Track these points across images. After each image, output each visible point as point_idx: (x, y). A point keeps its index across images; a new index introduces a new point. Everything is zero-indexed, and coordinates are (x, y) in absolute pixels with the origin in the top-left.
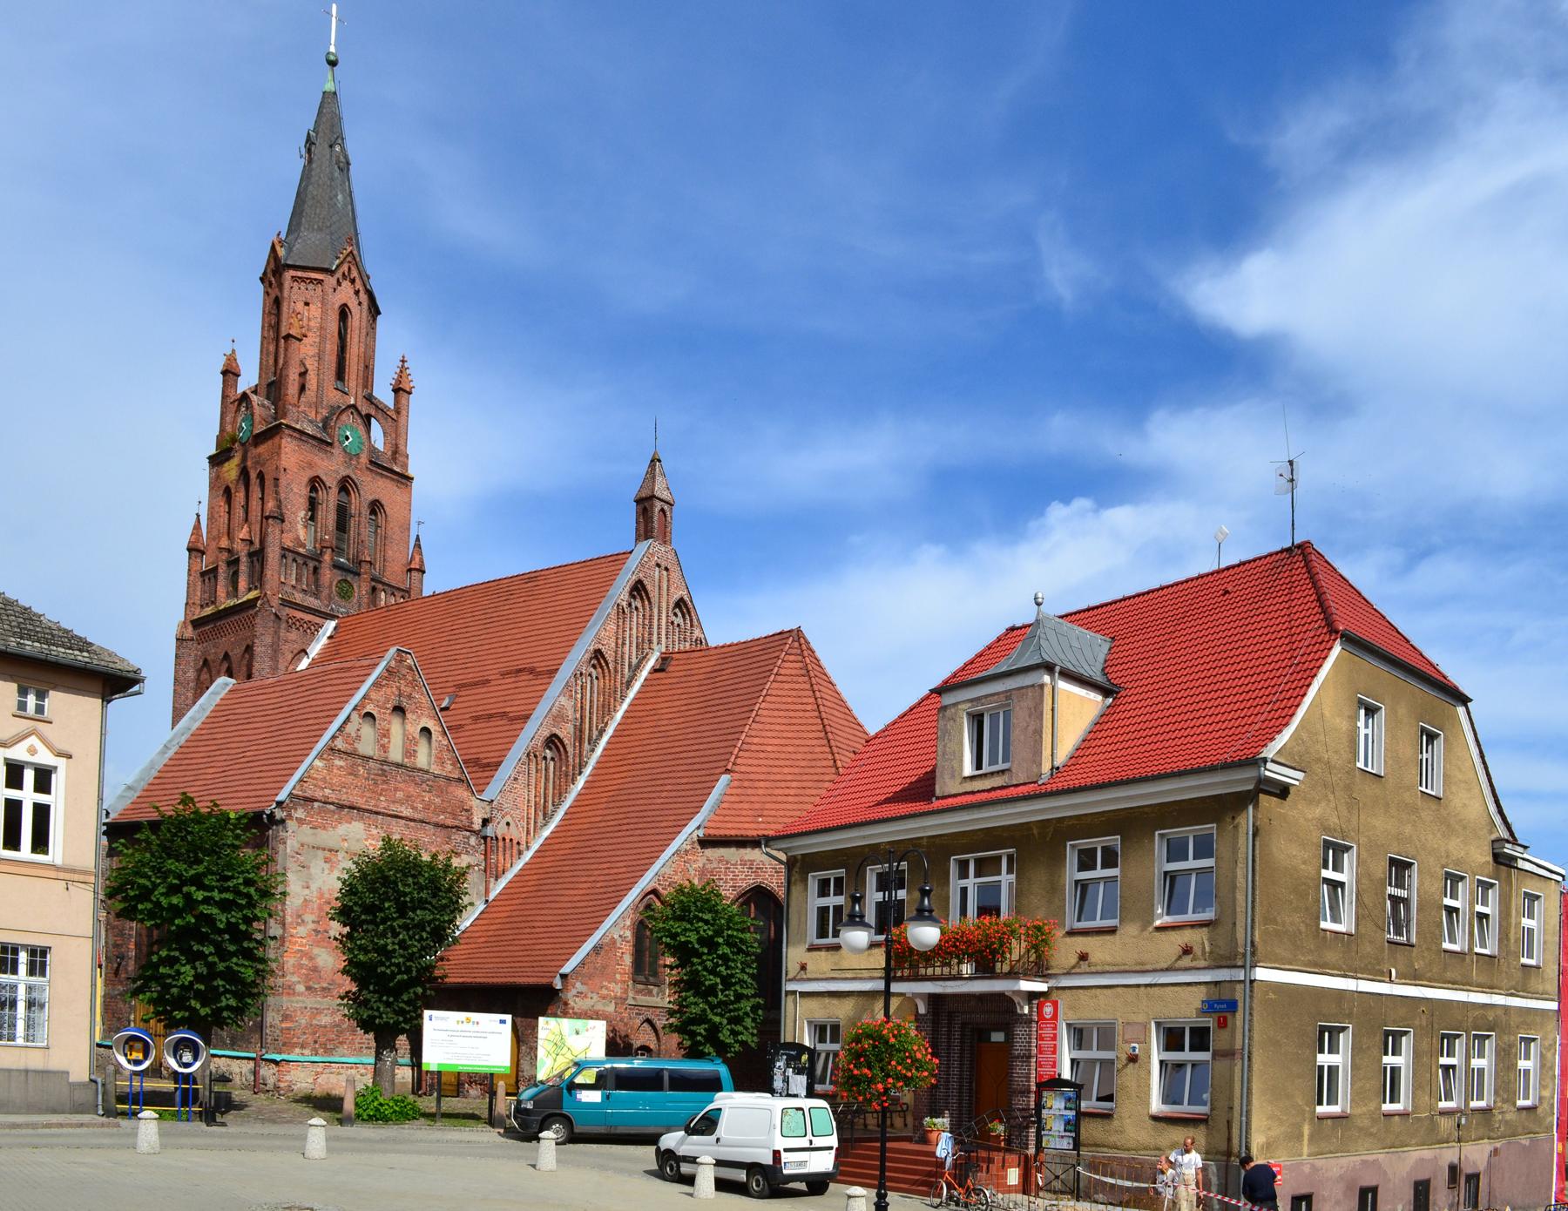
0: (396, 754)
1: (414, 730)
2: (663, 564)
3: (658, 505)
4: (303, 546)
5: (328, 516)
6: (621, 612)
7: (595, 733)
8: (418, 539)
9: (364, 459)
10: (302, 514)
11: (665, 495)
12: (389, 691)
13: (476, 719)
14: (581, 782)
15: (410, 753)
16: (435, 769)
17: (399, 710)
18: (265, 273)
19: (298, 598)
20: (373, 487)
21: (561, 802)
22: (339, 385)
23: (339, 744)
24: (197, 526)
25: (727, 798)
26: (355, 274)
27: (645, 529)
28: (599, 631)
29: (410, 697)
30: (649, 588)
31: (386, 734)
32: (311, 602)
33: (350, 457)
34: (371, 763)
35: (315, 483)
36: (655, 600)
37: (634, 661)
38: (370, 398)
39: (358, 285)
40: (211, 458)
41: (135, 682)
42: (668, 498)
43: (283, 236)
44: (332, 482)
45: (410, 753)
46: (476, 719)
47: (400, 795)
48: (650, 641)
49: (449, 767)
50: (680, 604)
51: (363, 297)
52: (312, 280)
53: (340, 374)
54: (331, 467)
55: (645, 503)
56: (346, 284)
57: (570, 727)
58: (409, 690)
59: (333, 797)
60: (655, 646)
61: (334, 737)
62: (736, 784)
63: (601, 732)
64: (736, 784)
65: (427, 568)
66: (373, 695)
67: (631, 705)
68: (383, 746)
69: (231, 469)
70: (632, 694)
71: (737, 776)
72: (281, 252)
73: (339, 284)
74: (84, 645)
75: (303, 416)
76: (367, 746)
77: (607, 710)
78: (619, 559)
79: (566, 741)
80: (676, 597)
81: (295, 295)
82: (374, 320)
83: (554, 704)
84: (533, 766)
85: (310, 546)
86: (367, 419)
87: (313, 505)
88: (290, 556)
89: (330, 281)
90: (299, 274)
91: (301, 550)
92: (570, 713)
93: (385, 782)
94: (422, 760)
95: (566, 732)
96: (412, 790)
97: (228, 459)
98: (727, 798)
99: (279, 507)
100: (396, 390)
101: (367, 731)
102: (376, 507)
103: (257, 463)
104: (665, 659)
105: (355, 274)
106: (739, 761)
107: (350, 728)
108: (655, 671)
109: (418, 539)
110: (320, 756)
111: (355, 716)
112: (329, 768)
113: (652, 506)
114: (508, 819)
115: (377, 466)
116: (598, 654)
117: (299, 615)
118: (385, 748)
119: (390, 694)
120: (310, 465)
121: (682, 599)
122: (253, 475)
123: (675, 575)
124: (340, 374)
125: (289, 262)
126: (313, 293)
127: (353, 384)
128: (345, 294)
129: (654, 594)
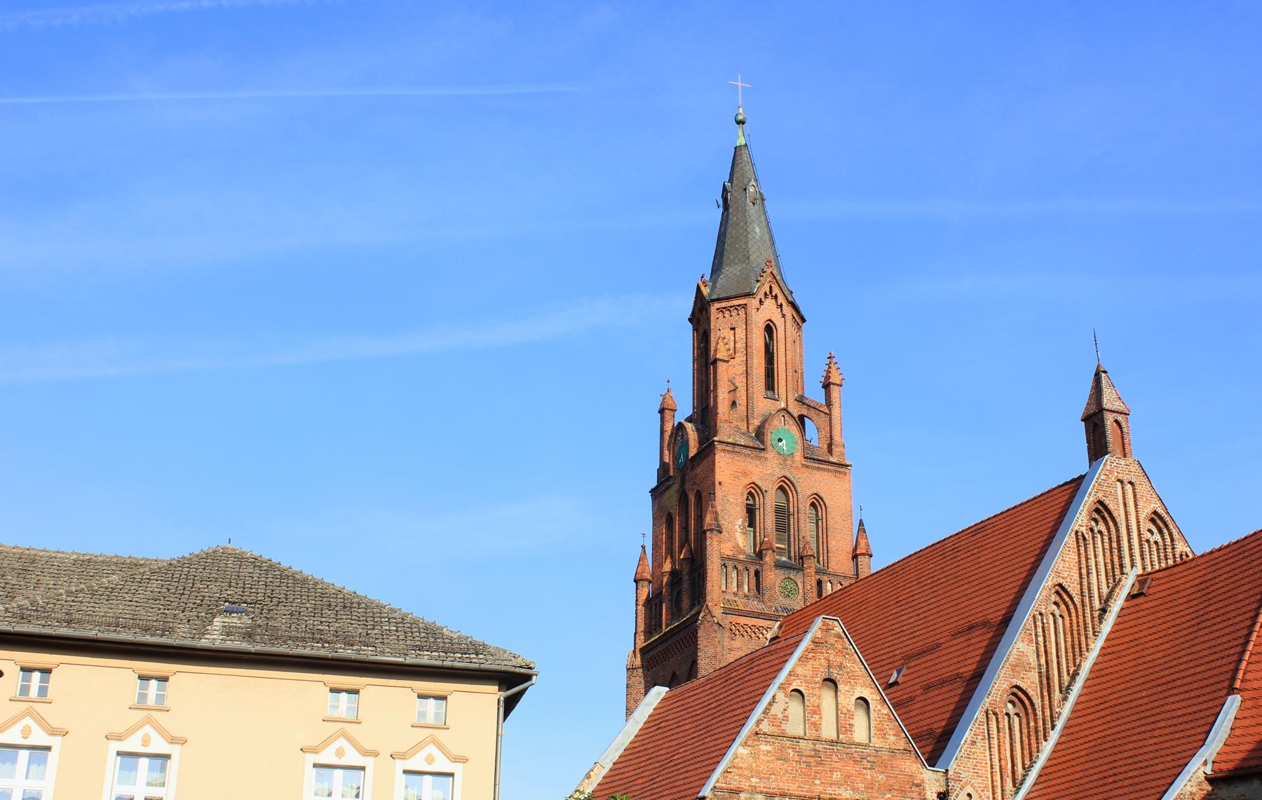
0: (828, 730)
1: (848, 698)
2: (1126, 478)
3: (1109, 419)
4: (742, 552)
5: (768, 519)
6: (1080, 538)
7: (1066, 678)
8: (861, 523)
9: (798, 457)
10: (740, 521)
11: (1117, 405)
12: (816, 663)
13: (927, 688)
14: (1054, 736)
15: (843, 726)
16: (876, 742)
17: (831, 682)
18: (693, 314)
19: (741, 604)
20: (811, 482)
21: (1032, 763)
22: (770, 394)
23: (765, 727)
24: (642, 558)
25: (1239, 723)
26: (776, 290)
27: (1097, 448)
28: (1063, 565)
29: (841, 667)
30: (1111, 507)
31: (817, 710)
32: (755, 605)
33: (784, 458)
34: (802, 743)
35: (754, 492)
36: (1121, 520)
37: (1105, 591)
38: (801, 400)
39: (781, 299)
40: (652, 491)
41: (527, 678)
42: (1122, 408)
43: (707, 278)
44: (771, 487)
45: (843, 726)
46: (927, 688)
47: (837, 776)
48: (1121, 566)
49: (892, 738)
50: (1156, 518)
51: (788, 310)
52: (736, 307)
53: (770, 384)
54: (766, 472)
55: (1094, 421)
56: (769, 302)
57: (1035, 676)
58: (839, 659)
59: (761, 785)
60: (1127, 569)
61: (759, 722)
62: (1249, 704)
63: (1073, 677)
64: (1249, 704)
65: (873, 551)
66: (799, 671)
67: (1107, 640)
68: (814, 724)
69: (672, 496)
70: (1107, 627)
71: (1248, 694)
72: (706, 291)
73: (761, 302)
74: (478, 649)
75: (729, 426)
76: (795, 726)
77: (1078, 651)
78: (1077, 484)
79: (1031, 693)
80: (1149, 510)
81: (720, 324)
82: (799, 327)
83: (1020, 655)
84: (993, 725)
85: (750, 551)
86: (801, 420)
87: (751, 511)
88: (730, 564)
89: (754, 303)
90: (724, 304)
91: (741, 557)
92: (1032, 659)
93: (819, 764)
94: (860, 734)
95: (1030, 682)
96: (851, 769)
97: (668, 488)
98: (1239, 723)
99: (716, 519)
100: (827, 386)
101: (795, 708)
102: (817, 503)
103: (694, 483)
104: (1142, 580)
105: (776, 290)
106: (1248, 676)
107: (776, 710)
108: (1131, 597)
109: (861, 523)
110: (745, 744)
111: (781, 697)
112: (755, 756)
113: (1102, 420)
114: (969, 789)
115: (811, 458)
116: (1061, 589)
117: (742, 620)
118: (816, 726)
119: (818, 668)
120: (745, 474)
121: (1155, 513)
122: (692, 498)
123: (1143, 489)
124: (770, 384)
125: (714, 297)
126: (737, 319)
127: (782, 391)
128: (769, 310)
129: (1119, 514)
